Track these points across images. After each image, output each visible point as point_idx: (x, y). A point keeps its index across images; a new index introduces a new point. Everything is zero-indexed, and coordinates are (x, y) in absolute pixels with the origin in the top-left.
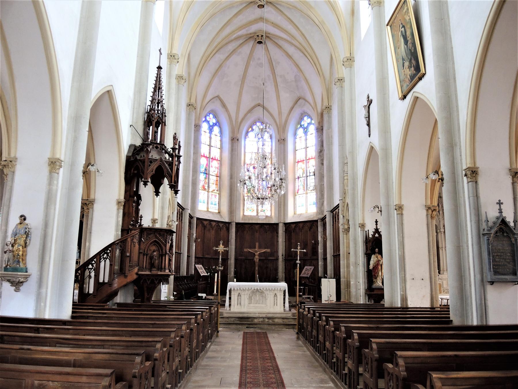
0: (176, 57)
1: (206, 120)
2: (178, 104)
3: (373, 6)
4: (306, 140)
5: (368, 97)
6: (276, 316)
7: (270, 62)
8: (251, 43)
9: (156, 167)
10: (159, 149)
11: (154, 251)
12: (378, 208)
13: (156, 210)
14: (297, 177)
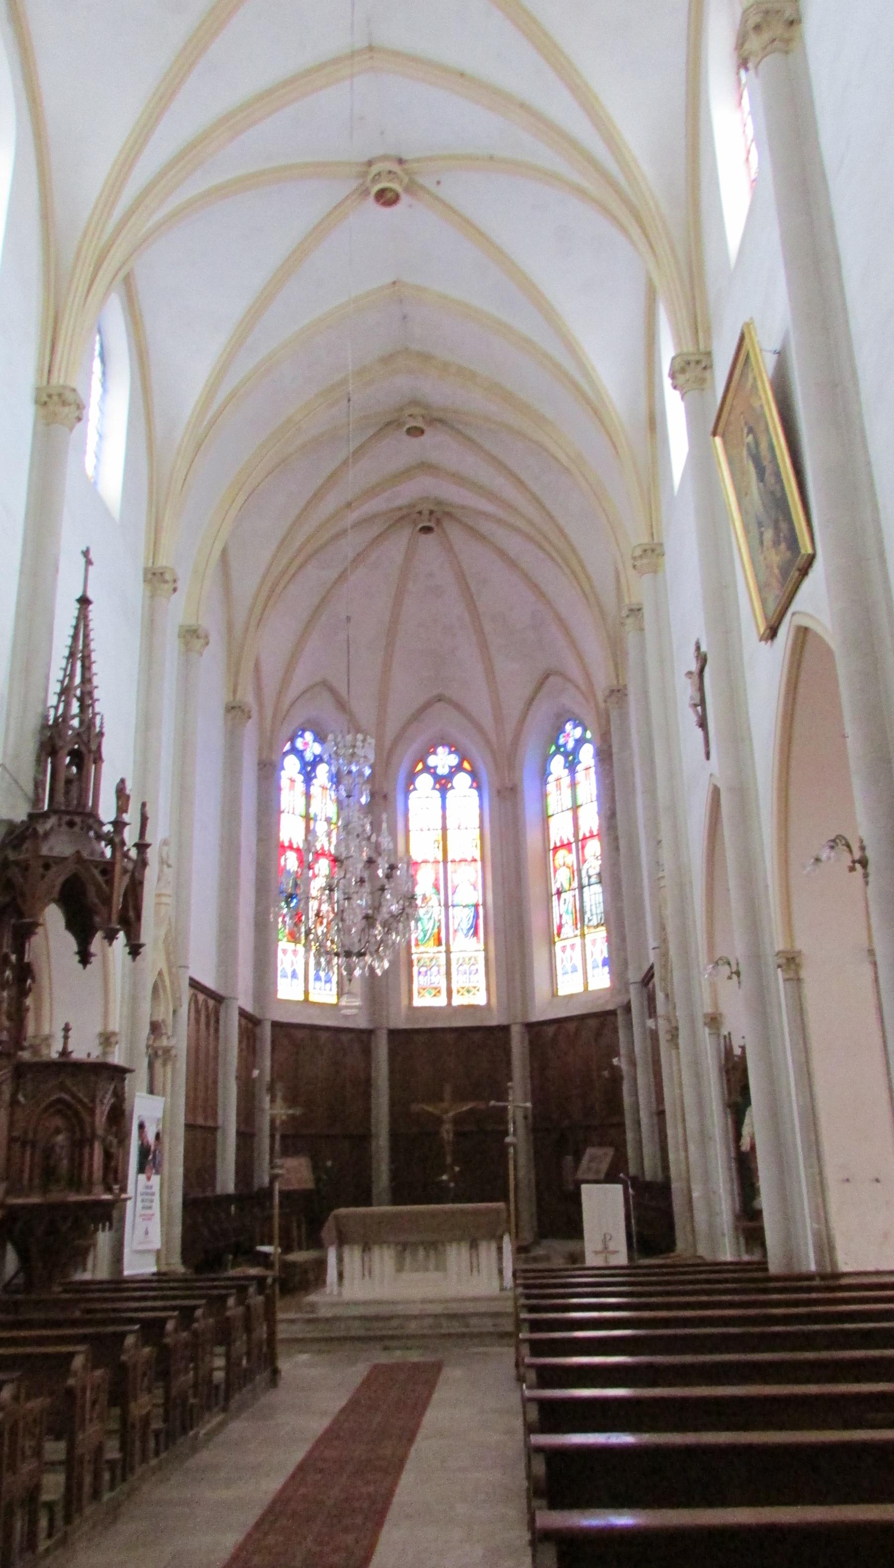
0: (167, 577)
1: (294, 750)
4: (573, 785)
5: (698, 648)
6: (470, 1307)
7: (461, 577)
8: (405, 534)
9: (61, 880)
10: (77, 829)
11: (58, 1131)
12: (729, 964)
13: (111, 1006)
14: (554, 891)
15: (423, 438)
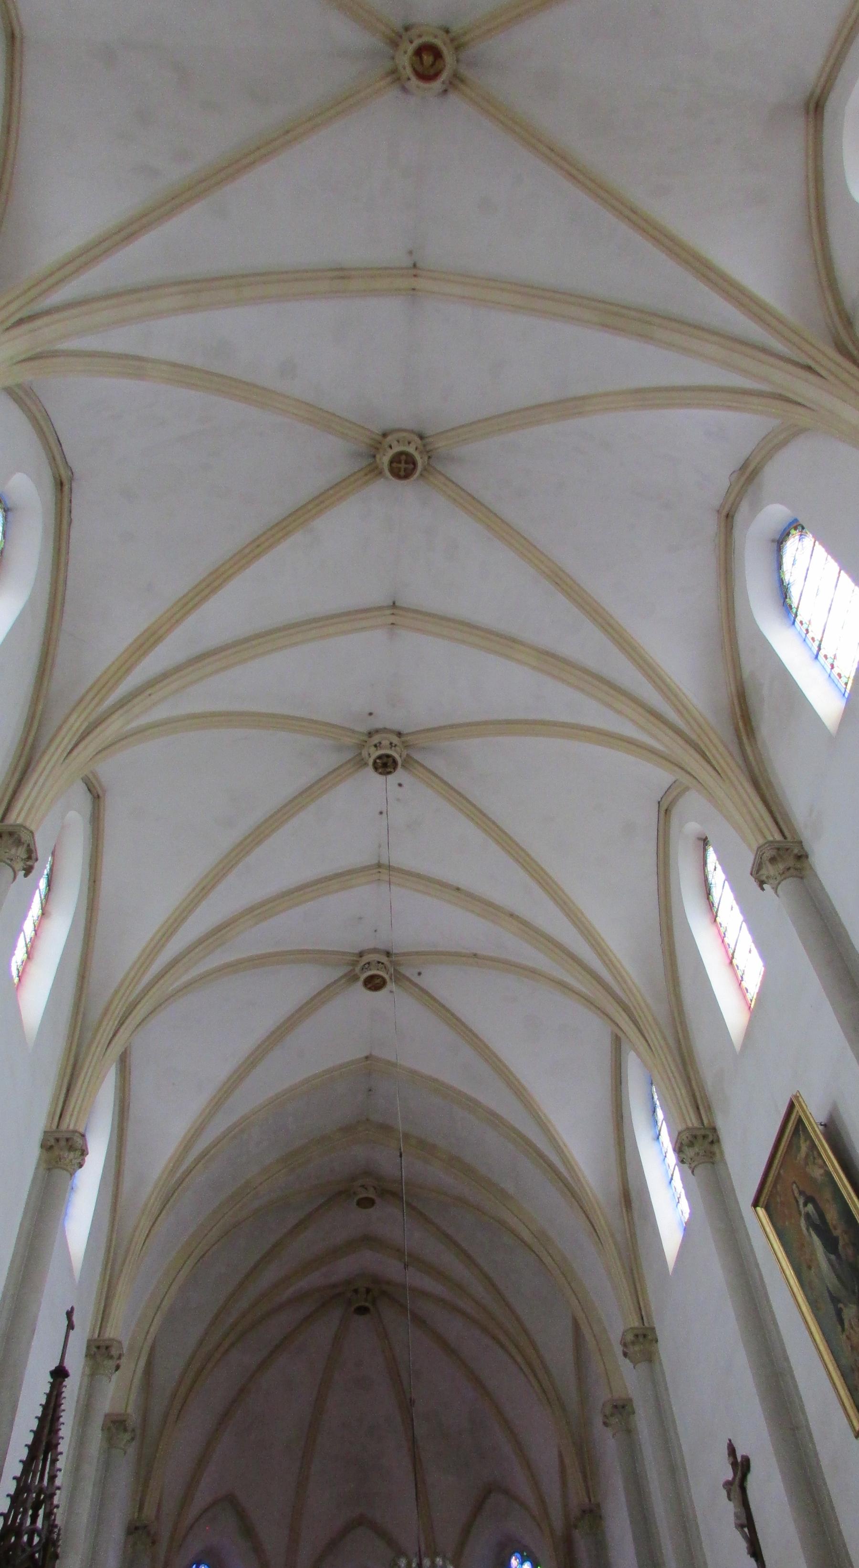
0: (114, 1352)
2: (99, 1519)
3: (693, 1165)
5: (732, 1451)
15: (371, 1210)
